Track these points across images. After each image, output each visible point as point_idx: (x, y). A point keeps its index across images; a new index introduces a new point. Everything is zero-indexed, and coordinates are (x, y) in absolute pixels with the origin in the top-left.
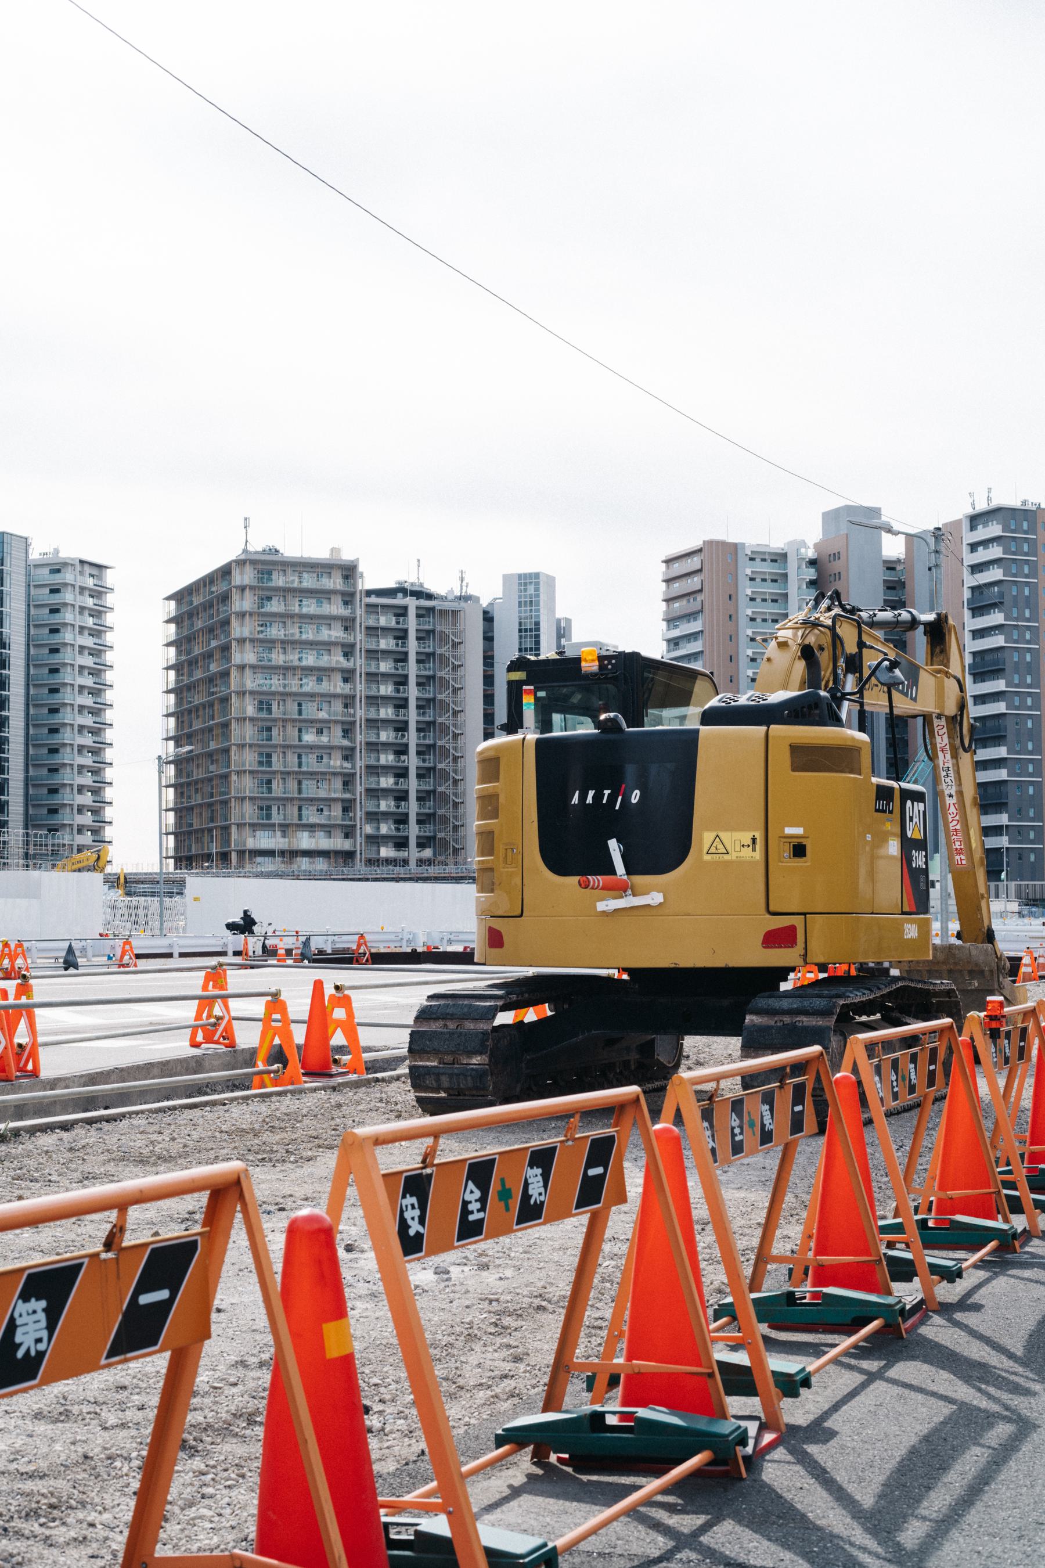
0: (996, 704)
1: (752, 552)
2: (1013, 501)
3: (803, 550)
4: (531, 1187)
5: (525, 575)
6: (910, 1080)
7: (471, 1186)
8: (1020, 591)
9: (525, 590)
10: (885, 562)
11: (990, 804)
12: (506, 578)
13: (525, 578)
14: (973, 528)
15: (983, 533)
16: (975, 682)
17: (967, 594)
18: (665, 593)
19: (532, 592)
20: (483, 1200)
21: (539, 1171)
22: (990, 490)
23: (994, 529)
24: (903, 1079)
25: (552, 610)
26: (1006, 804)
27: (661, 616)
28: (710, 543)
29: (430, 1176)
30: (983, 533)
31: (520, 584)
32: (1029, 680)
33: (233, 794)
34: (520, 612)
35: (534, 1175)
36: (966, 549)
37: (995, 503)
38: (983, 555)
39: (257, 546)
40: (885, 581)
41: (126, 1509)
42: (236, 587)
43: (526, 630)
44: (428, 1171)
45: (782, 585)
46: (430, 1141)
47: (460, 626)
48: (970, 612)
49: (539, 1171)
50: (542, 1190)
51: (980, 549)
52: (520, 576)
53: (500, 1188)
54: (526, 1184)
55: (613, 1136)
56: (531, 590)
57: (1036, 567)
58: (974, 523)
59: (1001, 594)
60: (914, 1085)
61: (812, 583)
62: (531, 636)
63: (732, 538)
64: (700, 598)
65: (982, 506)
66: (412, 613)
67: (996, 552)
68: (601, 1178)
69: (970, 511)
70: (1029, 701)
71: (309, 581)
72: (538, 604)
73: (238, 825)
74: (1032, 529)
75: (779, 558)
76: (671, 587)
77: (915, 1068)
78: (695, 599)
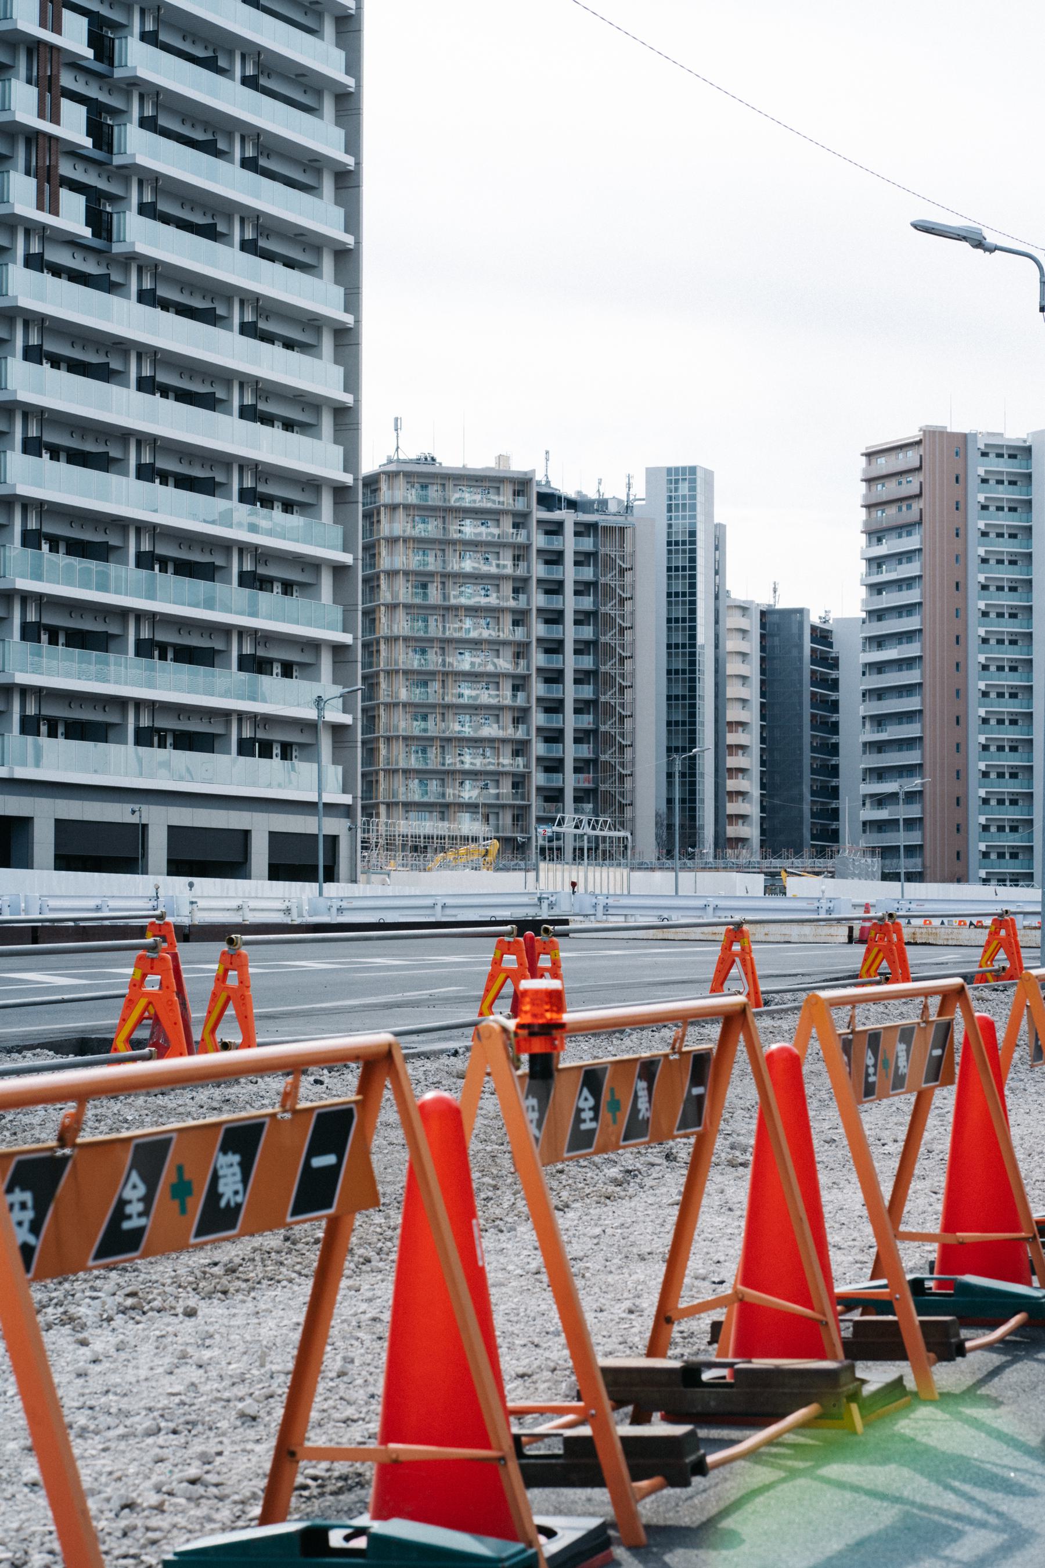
1: (986, 445)
4: (222, 1182)
5: (677, 469)
6: (897, 1068)
7: (135, 1177)
9: (676, 489)
12: (651, 473)
13: (677, 474)
19: (686, 492)
20: (147, 1200)
21: (236, 1159)
25: (710, 515)
29: (65, 1159)
31: (670, 482)
33: (381, 766)
35: (229, 1165)
39: (410, 451)
42: (385, 506)
43: (677, 543)
44: (67, 1151)
45: (1024, 489)
46: (71, 1107)
47: (628, 548)
49: (236, 1159)
50: (239, 1187)
52: (669, 470)
53: (174, 1179)
54: (215, 1178)
55: (350, 1110)
56: (684, 489)
60: (903, 1077)
62: (684, 628)
63: (957, 426)
64: (916, 506)
66: (569, 529)
68: (332, 1172)
71: (470, 498)
72: (693, 507)
73: (388, 805)
76: (873, 488)
77: (908, 1051)
78: (909, 507)
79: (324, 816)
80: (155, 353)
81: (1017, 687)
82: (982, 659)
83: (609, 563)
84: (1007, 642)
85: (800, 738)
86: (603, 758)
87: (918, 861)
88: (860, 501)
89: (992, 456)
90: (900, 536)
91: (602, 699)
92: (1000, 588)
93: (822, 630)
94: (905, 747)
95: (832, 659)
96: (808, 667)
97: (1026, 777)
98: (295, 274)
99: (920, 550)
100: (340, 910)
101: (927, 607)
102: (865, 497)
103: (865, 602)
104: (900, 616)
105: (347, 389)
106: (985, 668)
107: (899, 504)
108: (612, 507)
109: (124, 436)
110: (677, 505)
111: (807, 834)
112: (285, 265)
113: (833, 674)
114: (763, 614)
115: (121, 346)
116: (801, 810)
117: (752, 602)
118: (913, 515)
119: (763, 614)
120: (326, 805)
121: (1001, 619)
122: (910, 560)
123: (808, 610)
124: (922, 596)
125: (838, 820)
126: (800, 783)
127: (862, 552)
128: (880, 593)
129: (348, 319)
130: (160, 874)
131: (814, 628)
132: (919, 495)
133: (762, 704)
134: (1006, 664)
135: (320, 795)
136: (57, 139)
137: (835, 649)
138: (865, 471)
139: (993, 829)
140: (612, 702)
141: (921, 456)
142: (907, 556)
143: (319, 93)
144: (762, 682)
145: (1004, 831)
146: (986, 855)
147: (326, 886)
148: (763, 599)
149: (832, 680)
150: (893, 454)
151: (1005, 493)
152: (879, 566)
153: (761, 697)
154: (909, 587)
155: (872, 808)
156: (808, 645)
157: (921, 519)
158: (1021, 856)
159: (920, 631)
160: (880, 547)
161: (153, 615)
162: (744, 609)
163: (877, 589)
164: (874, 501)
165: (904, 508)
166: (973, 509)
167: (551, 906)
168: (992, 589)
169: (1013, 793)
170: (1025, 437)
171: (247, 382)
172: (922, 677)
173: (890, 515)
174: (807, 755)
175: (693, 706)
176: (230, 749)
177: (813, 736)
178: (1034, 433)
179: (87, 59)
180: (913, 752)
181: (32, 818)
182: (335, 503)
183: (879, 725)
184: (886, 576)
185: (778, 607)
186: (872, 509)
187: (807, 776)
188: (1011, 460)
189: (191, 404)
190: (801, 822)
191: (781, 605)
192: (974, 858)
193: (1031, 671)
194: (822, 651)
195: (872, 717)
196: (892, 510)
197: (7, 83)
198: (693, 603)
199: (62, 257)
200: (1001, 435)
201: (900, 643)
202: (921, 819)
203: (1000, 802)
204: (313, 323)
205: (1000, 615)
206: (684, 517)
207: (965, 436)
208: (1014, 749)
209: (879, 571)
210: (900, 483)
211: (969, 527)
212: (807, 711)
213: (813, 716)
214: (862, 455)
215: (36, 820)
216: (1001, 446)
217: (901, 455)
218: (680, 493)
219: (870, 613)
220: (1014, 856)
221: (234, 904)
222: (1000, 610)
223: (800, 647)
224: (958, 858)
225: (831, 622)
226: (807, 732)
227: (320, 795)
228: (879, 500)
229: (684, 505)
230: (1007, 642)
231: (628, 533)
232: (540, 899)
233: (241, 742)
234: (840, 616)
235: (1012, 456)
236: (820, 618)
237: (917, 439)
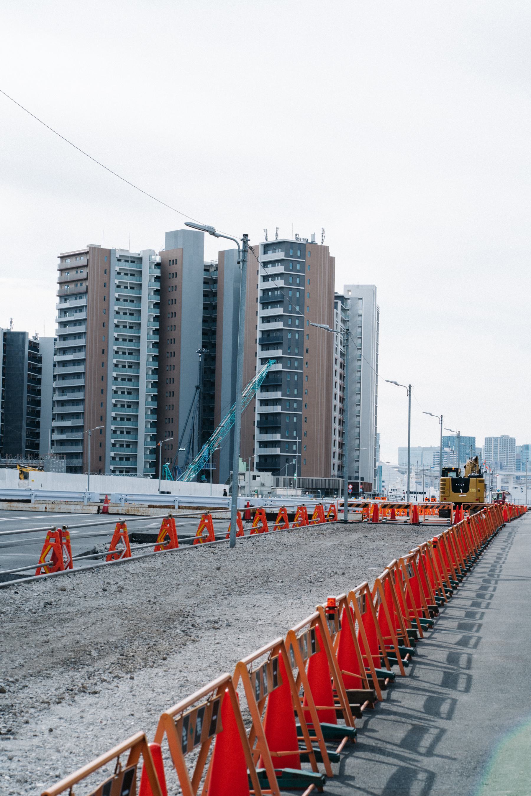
0: (276, 351)
1: (120, 256)
2: (291, 238)
3: (153, 257)
8: (294, 295)
10: (205, 266)
11: (269, 427)
14: (265, 252)
15: (271, 256)
16: (262, 350)
17: (260, 294)
22: (277, 229)
23: (280, 255)
24: (191, 731)
26: (280, 427)
27: (56, 293)
30: (271, 256)
32: (299, 254)
36: (260, 279)
37: (281, 238)
38: (271, 270)
40: (204, 278)
45: (138, 278)
48: (261, 305)
51: (270, 266)
57: (304, 280)
58: (266, 249)
59: (282, 296)
61: (157, 278)
64: (85, 284)
65: (272, 239)
67: (280, 269)
69: (264, 241)
70: (297, 322)
74: (303, 256)
75: (138, 260)
76: (63, 274)
77: (201, 721)
78: (81, 284)
81: (132, 349)
82: (115, 361)
84: (126, 380)
85: (22, 397)
87: (80, 460)
90: (76, 299)
92: (125, 327)
93: (34, 343)
94: (76, 390)
95: (39, 357)
96: (27, 361)
97: (136, 394)
99: (86, 306)
101: (89, 334)
102: (59, 278)
103: (58, 331)
104: (75, 325)
106: (116, 366)
107: (76, 283)
111: (24, 446)
113: (39, 365)
114: (5, 334)
116: (21, 435)
118: (83, 288)
119: (5, 334)
121: (125, 342)
122: (81, 311)
123: (28, 333)
124: (86, 329)
125: (40, 417)
126: (21, 420)
127: (57, 306)
128: (65, 326)
131: (30, 342)
132: (86, 279)
134: (125, 404)
138: (59, 265)
139: (118, 446)
141: (88, 260)
142: (79, 309)
145: (123, 447)
146: (114, 445)
149: (38, 379)
150: (74, 258)
152: (65, 313)
153: (3, 376)
154: (80, 324)
155: (58, 434)
156: (27, 350)
157: (87, 291)
158: (131, 433)
159: (85, 346)
163: (63, 324)
164: (63, 281)
165: (79, 285)
166: (113, 287)
168: (121, 327)
169: (128, 428)
172: (85, 383)
174: (25, 405)
177: (28, 396)
178: (144, 251)
180: (78, 460)
183: (63, 392)
185: (12, 331)
186: (63, 285)
187: (25, 416)
188: (132, 264)
190: (21, 439)
193: (139, 355)
194: (34, 354)
195: (59, 388)
196: (73, 286)
200: (127, 251)
201: (75, 352)
202: (83, 413)
203: (122, 432)
205: (124, 353)
207: (110, 251)
208: (129, 420)
209: (65, 316)
210: (77, 272)
211: (110, 336)
212: (26, 383)
213: (29, 386)
214: (58, 257)
216: (127, 257)
217: (78, 259)
219: (60, 336)
220: (128, 459)
223: (23, 351)
225: (38, 339)
226: (25, 394)
228: (66, 280)
230: (126, 380)
235: (133, 262)
236: (33, 337)
237: (86, 251)
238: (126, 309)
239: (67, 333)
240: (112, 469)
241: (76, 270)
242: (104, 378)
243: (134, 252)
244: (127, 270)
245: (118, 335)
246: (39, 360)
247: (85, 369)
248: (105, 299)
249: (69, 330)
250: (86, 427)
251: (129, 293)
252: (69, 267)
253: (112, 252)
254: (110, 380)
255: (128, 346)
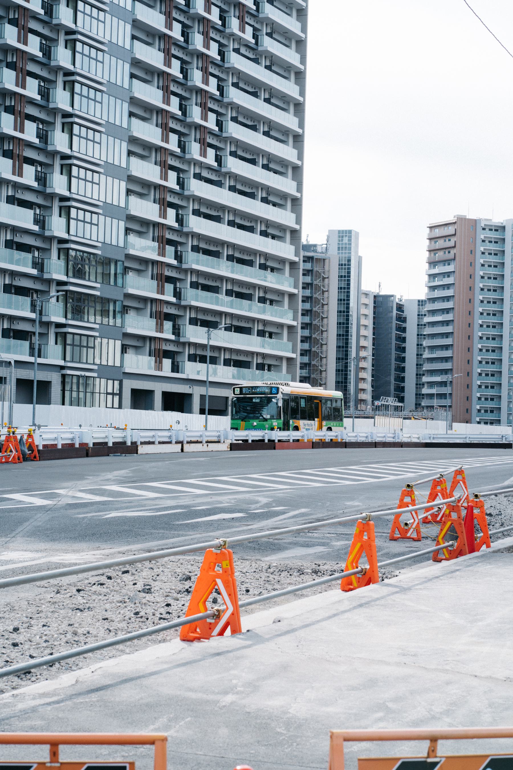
1: (485, 225)
5: (343, 231)
9: (342, 240)
13: (343, 233)
18: (429, 246)
19: (347, 242)
25: (357, 252)
28: (461, 221)
31: (339, 237)
34: (339, 253)
41: (324, 622)
45: (501, 245)
56: (346, 240)
72: (350, 249)
78: (449, 252)
79: (209, 387)
80: (200, 199)
83: (318, 275)
86: (313, 363)
88: (426, 248)
89: (487, 230)
90: (444, 265)
91: (313, 336)
92: (489, 302)
93: (400, 304)
95: (404, 318)
98: (277, 176)
100: (434, 438)
103: (427, 294)
105: (297, 223)
107: (444, 250)
108: (319, 249)
109: (223, 243)
110: (342, 248)
112: (274, 173)
115: (223, 208)
117: (370, 291)
120: (210, 382)
125: (404, 392)
126: (390, 375)
127: (426, 272)
129: (298, 195)
130: (57, 404)
132: (455, 247)
133: (373, 338)
135: (207, 378)
136: (26, 53)
137: (405, 314)
139: (483, 411)
140: (318, 338)
141: (456, 229)
143: (288, 103)
144: (374, 328)
145: (487, 412)
147: (39, 408)
148: (374, 290)
149: (402, 377)
150: (442, 228)
151: (493, 247)
157: (455, 258)
160: (434, 270)
161: (264, 321)
162: (366, 295)
163: (432, 288)
164: (433, 248)
167: (506, 439)
168: (486, 278)
170: (502, 221)
171: (263, 221)
173: (440, 255)
175: (347, 339)
176: (282, 369)
178: (507, 220)
179: (180, 78)
181: (51, 382)
182: (290, 269)
184: (437, 283)
188: (495, 256)
189: (210, 220)
191: (382, 293)
192: (474, 412)
193: (500, 413)
197: (3, 25)
198: (348, 292)
199: (205, 174)
200: (491, 220)
204: (284, 196)
206: (345, 253)
207: (476, 220)
209: (434, 281)
215: (155, 392)
216: (492, 226)
217: (446, 228)
218: (344, 242)
221: (383, 435)
222: (489, 300)
224: (467, 412)
225: (403, 301)
227: (207, 378)
229: (346, 247)
231: (327, 261)
232: (502, 436)
233: (225, 360)
234: (407, 298)
235: (496, 230)
237: (454, 221)
238: (491, 274)
239: (436, 296)
240: (478, 420)
241: (445, 238)
242: (470, 374)
243: (497, 221)
244: (491, 250)
245: (482, 346)
246: (404, 320)
247: (453, 329)
248: (471, 265)
249: (437, 294)
250: (454, 370)
251: (493, 259)
252: (437, 236)
253: (477, 221)
254: (476, 339)
255: (491, 356)
